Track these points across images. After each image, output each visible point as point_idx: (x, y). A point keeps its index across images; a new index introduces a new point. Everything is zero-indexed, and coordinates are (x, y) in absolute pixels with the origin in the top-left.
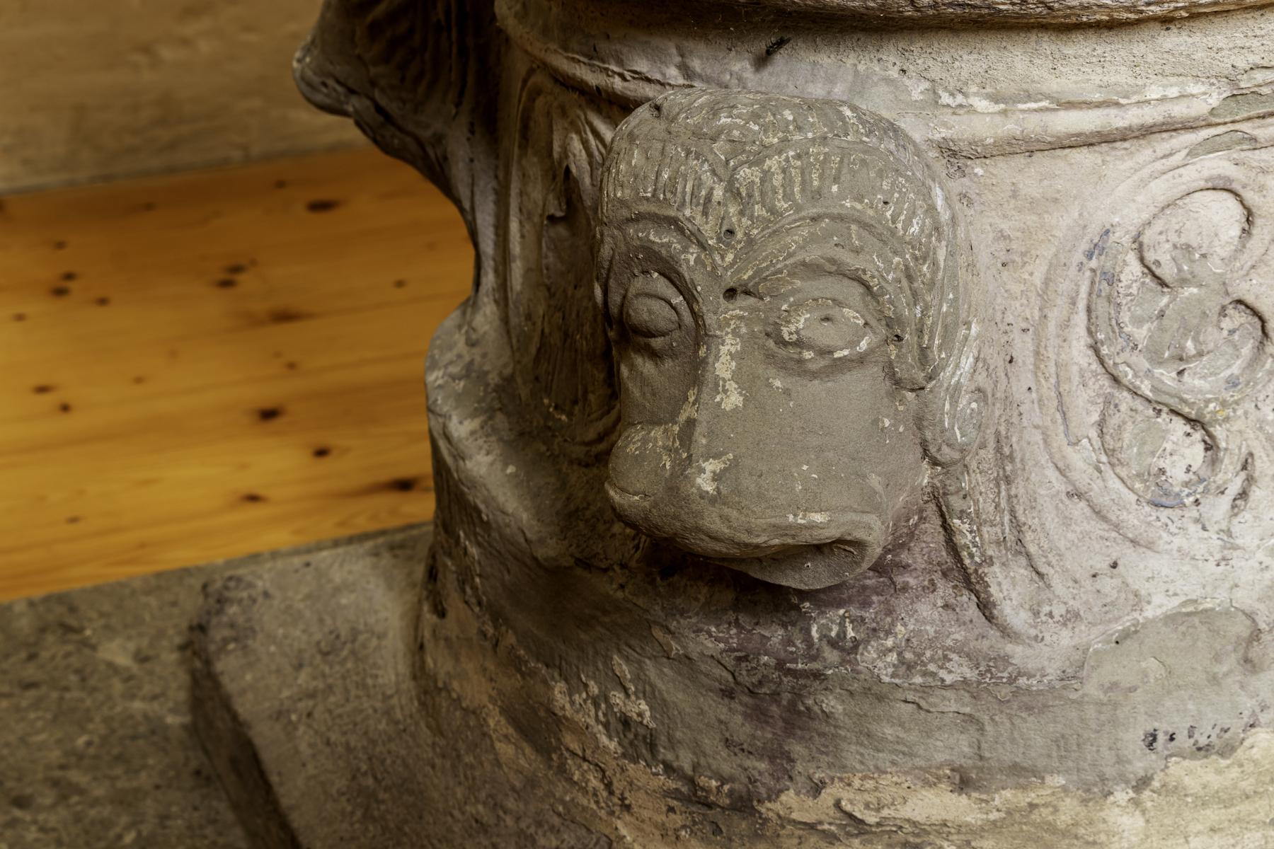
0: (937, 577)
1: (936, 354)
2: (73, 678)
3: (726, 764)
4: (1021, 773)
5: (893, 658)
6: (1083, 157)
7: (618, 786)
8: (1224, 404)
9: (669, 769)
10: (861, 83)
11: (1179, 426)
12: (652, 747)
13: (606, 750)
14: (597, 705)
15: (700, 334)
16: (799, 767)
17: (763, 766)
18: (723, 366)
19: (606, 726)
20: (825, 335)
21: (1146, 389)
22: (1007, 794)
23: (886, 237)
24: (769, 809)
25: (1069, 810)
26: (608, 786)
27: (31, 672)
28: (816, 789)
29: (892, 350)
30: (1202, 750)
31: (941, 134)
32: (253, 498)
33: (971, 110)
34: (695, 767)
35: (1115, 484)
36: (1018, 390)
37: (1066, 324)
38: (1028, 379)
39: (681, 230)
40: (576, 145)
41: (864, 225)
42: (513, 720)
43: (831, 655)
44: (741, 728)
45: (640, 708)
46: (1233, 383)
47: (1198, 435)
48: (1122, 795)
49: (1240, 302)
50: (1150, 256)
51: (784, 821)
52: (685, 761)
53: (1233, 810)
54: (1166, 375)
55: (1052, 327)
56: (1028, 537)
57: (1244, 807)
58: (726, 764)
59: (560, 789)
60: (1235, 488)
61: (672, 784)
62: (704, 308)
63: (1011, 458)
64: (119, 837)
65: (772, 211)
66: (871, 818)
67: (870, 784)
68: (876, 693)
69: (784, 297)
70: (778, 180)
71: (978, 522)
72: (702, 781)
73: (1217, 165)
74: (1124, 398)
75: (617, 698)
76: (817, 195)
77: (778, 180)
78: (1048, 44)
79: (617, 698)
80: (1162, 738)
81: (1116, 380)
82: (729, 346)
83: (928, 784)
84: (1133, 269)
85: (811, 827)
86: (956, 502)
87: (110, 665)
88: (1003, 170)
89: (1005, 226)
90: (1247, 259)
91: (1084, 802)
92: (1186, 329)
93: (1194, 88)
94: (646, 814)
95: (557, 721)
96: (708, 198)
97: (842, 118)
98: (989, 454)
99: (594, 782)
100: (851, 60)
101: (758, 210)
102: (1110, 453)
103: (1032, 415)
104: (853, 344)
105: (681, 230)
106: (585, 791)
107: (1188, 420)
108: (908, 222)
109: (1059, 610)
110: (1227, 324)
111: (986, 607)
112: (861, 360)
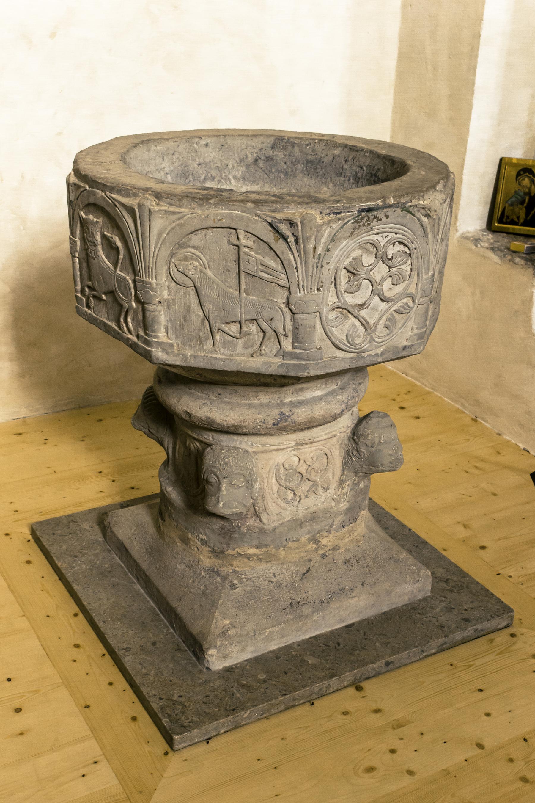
0: (253, 516)
1: (254, 484)
2: (78, 532)
3: (219, 545)
4: (267, 546)
6: (274, 453)
7: (200, 550)
8: (296, 487)
9: (209, 547)
10: (241, 443)
11: (289, 491)
12: (206, 543)
13: (198, 544)
14: (197, 537)
15: (220, 483)
16: (231, 546)
17: (225, 546)
18: (223, 488)
19: (198, 540)
20: (238, 483)
21: (284, 486)
22: (264, 549)
23: (247, 469)
24: (226, 553)
25: (273, 551)
26: (199, 550)
27: (69, 531)
28: (234, 549)
29: (247, 484)
30: (294, 541)
31: (253, 450)
32: (101, 492)
33: (258, 446)
34: (214, 546)
35: (280, 500)
36: (265, 487)
37: (272, 477)
38: (266, 485)
39: (217, 468)
40: (192, 445)
41: (243, 467)
42: (181, 540)
43: (237, 528)
44: (222, 540)
45: (205, 537)
47: (292, 492)
48: (282, 548)
49: (298, 472)
50: (285, 466)
51: (229, 554)
52: (212, 545)
53: (352, 258)
54: (288, 484)
55: (270, 477)
56: (267, 509)
58: (219, 545)
59: (190, 550)
60: (298, 500)
61: (210, 549)
62: (220, 479)
63: (264, 497)
64: (96, 562)
65: (230, 466)
66: (243, 554)
67: (242, 548)
68: (244, 534)
69: (232, 478)
70: (231, 461)
71: (259, 507)
72: (215, 549)
73: (295, 452)
74: (281, 488)
75: (201, 536)
76: (237, 463)
77: (231, 461)
78: (269, 437)
79: (201, 536)
80: (288, 540)
82: (224, 485)
83: (251, 548)
84: (282, 468)
85: (233, 555)
86: (256, 505)
87: (85, 529)
88: (263, 455)
91: (276, 550)
92: (290, 477)
93: (291, 442)
94: (205, 554)
95: (189, 539)
96: (221, 464)
97: (240, 451)
98: (261, 497)
99: (196, 549)
100: (239, 438)
101: (228, 466)
102: (279, 495)
103: (267, 491)
104: (242, 484)
105: (217, 468)
106: (194, 551)
107: (291, 490)
108: (250, 466)
109: (272, 520)
110: (296, 475)
111: (261, 520)
112: (243, 486)
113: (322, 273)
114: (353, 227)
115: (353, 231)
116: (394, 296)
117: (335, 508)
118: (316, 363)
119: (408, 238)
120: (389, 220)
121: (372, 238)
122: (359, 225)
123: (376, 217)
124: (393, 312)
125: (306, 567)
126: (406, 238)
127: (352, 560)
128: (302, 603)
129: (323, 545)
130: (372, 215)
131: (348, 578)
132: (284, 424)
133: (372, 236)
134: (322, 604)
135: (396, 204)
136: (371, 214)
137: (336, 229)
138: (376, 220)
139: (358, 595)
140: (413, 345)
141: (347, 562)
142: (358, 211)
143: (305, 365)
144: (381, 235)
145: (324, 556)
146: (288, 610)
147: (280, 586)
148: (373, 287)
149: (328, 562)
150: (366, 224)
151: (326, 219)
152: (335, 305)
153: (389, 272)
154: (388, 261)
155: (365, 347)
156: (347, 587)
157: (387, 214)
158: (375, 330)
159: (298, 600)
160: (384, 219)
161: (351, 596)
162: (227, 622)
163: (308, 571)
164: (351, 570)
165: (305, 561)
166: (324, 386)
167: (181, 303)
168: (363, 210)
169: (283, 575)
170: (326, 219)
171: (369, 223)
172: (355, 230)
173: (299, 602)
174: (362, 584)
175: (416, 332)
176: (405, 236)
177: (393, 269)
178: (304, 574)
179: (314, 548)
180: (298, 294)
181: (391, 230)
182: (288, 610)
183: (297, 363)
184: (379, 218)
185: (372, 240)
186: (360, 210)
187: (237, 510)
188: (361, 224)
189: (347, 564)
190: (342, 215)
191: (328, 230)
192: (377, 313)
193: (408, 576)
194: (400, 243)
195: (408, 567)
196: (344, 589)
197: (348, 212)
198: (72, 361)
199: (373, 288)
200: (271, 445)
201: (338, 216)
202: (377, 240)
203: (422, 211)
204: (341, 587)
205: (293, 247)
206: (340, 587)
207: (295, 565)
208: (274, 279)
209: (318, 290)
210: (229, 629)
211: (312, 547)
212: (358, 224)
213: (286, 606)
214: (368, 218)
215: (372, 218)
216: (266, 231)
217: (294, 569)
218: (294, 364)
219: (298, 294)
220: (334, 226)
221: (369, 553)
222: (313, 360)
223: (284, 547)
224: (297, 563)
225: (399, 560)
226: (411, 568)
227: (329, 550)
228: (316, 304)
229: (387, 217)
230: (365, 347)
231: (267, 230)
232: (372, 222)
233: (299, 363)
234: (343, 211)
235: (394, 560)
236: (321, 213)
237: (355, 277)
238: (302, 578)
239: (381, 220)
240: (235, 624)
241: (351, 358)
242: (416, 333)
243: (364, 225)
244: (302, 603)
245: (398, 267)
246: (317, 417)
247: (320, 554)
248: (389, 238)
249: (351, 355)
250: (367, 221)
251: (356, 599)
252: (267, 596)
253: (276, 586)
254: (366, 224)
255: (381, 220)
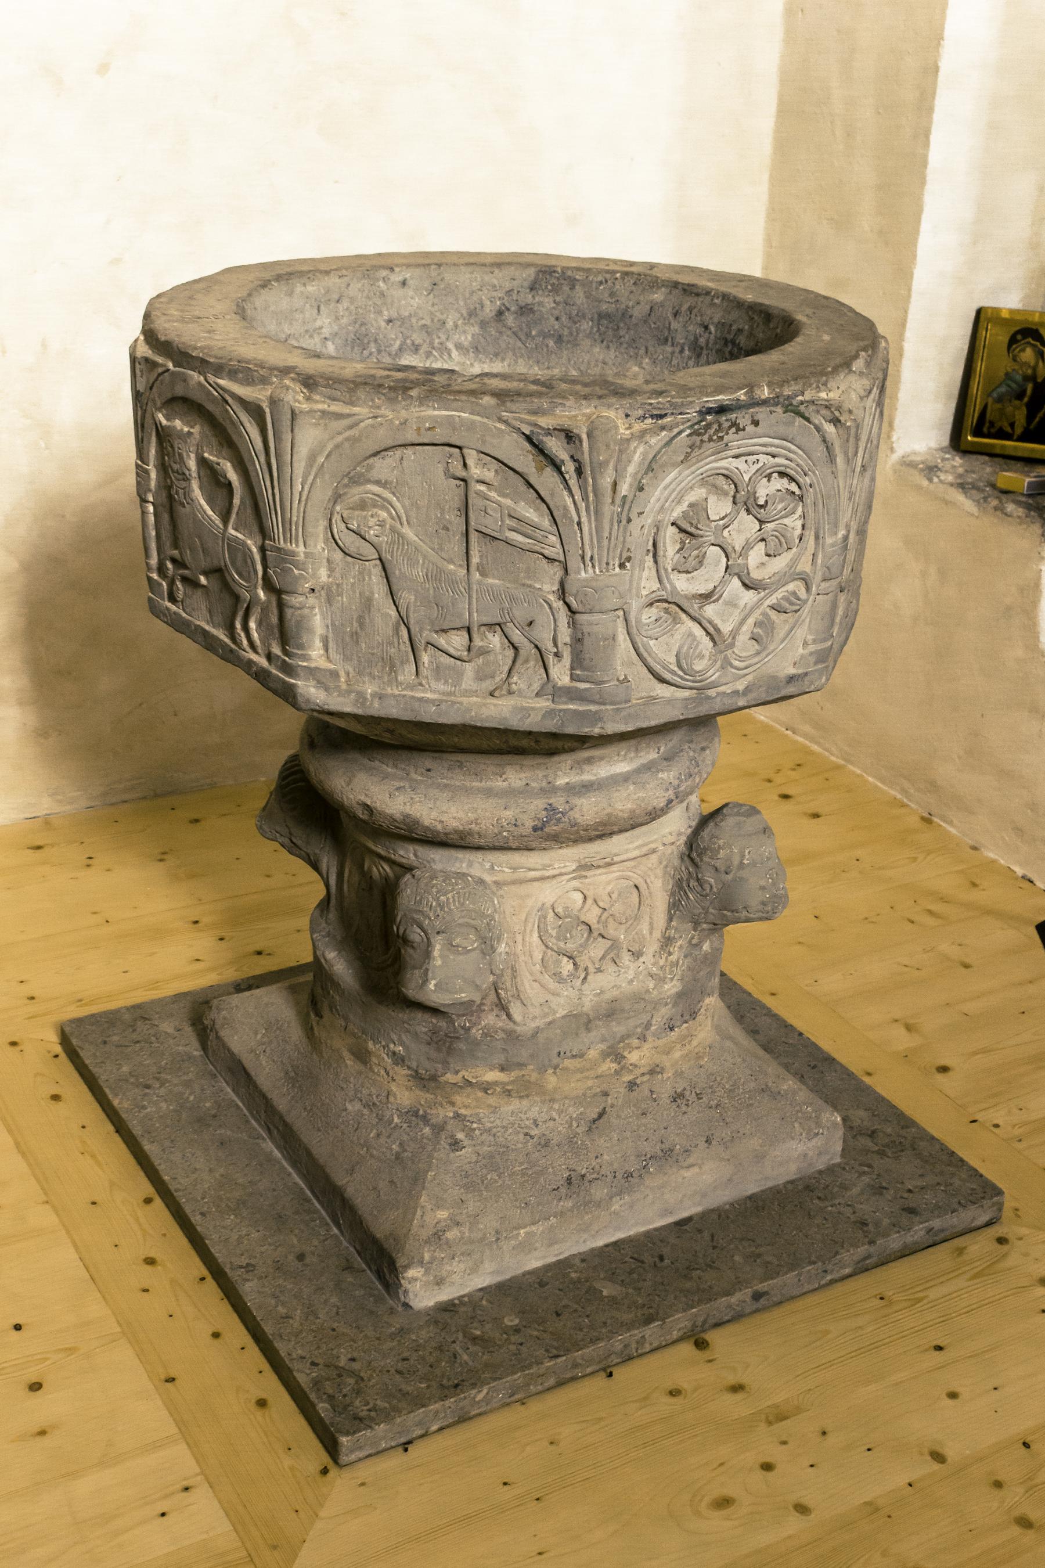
0: (494, 1007)
2: (153, 1039)
3: (427, 1064)
4: (521, 1065)
5: (481, 1032)
6: (535, 884)
7: (391, 1074)
8: (579, 952)
9: (409, 1068)
10: (470, 864)
11: (565, 959)
12: (403, 1061)
13: (387, 1062)
14: (384, 1049)
15: (429, 944)
16: (452, 1065)
17: (440, 1066)
18: (436, 953)
19: (387, 1055)
20: (465, 943)
21: (555, 948)
22: (516, 1072)
23: (483, 915)
24: (442, 1079)
25: (534, 1076)
26: (388, 1074)
27: (134, 1036)
28: (457, 1072)
30: (574, 1057)
31: (495, 878)
32: (198, 960)
33: (503, 872)
34: (417, 1067)
35: (547, 977)
36: (518, 951)
37: (532, 931)
38: (520, 947)
39: (423, 914)
40: (375, 869)
41: (476, 912)
42: (353, 1054)
43: (462, 1032)
44: (433, 1054)
45: (400, 1049)
46: (581, 946)
47: (571, 961)
48: (550, 1071)
49: (583, 922)
50: (556, 911)
51: (447, 1082)
52: (414, 1065)
53: (687, 503)
54: (562, 944)
55: (528, 931)
56: (521, 994)
57: (587, 1074)
58: (427, 1064)
59: (370, 1075)
60: (582, 976)
61: (409, 1072)
62: (431, 936)
64: (188, 1098)
65: (450, 909)
67: (473, 1070)
68: (477, 1044)
70: (451, 900)
71: (506, 990)
72: (420, 1071)
74: (549, 952)
75: (392, 1046)
77: (451, 900)
78: (526, 853)
79: (392, 1046)
80: (562, 1054)
81: (547, 947)
82: (438, 947)
83: (491, 1070)
84: (551, 914)
85: (455, 1084)
86: (500, 985)
88: (513, 888)
89: (513, 904)
90: (585, 910)
91: (539, 1073)
92: (567, 931)
93: (568, 864)
94: (400, 1082)
95: (368, 1053)
96: (431, 906)
97: (468, 880)
98: (509, 971)
99: (382, 1072)
100: (467, 856)
101: (446, 909)
102: (545, 967)
103: (522, 958)
105: (423, 914)
106: (379, 1075)
107: (568, 957)
108: (488, 910)
109: (531, 1016)
111: (509, 1016)
112: (474, 949)
113: (628, 534)
114: (690, 443)
115: (689, 450)
116: (770, 578)
117: (655, 992)
118: (618, 709)
119: (797, 465)
120: (759, 430)
121: (727, 465)
122: (701, 440)
123: (734, 424)
124: (768, 610)
125: (598, 1107)
126: (793, 465)
127: (687, 1093)
128: (589, 1177)
129: (631, 1065)
130: (727, 420)
131: (681, 1128)
132: (555, 828)
133: (726, 460)
134: (630, 1179)
135: (773, 398)
136: (724, 418)
137: (657, 448)
138: (733, 430)
139: (700, 1162)
140: (806, 674)
141: (677, 1097)
142: (700, 412)
143: (596, 712)
144: (744, 458)
145: (632, 1085)
146: (563, 1190)
147: (546, 1145)
148: (728, 560)
149: (640, 1098)
150: (715, 437)
151: (638, 427)
152: (654, 595)
153: (760, 530)
154: (759, 510)
155: (713, 678)
156: (678, 1147)
157: (756, 418)
158: (732, 645)
159: (583, 1172)
160: (750, 429)
161: (686, 1164)
162: (442, 1214)
163: (601, 1115)
164: (685, 1113)
165: (595, 1095)
166: (632, 754)
167: (354, 592)
168: (709, 411)
169: (552, 1122)
170: (638, 427)
171: (720, 435)
172: (693, 450)
173: (583, 1176)
174: (707, 1141)
175: (812, 648)
176: (791, 461)
177: (768, 525)
178: (594, 1121)
179: (613, 1070)
180: (583, 574)
181: (764, 449)
182: (563, 1190)
183: (581, 708)
184: (741, 426)
185: (727, 469)
186: (704, 409)
187: (463, 995)
188: (706, 438)
189: (679, 1101)
190: (669, 419)
191: (641, 449)
192: (737, 612)
193: (796, 1125)
194: (782, 474)
195: (798, 1108)
196: (672, 1151)
197: (681, 414)
198: (140, 705)
199: (729, 563)
200: (530, 870)
201: (660, 422)
202: (737, 468)
203: (824, 412)
204: (666, 1146)
205: (573, 482)
206: (663, 1146)
207: (575, 1104)
208: (535, 545)
209: (622, 566)
210: (448, 1228)
211: (609, 1069)
212: (700, 438)
213: (559, 1184)
214: (720, 426)
215: (726, 425)
216: (519, 452)
217: (574, 1112)
218: (575, 711)
219: (583, 574)
220: (653, 441)
221: (721, 1080)
222: (612, 704)
223: (556, 1067)
224: (580, 1100)
225: (779, 1093)
226: (804, 1110)
227: (643, 1074)
228: (617, 593)
229: (756, 423)
230: (713, 678)
231: (522, 449)
232: (727, 434)
233: (585, 708)
234: (670, 412)
235: (769, 1093)
236: (627, 416)
237: (694, 541)
238: (590, 1129)
239: (744, 429)
240: (459, 1218)
241: (686, 699)
242: (813, 650)
243: (710, 440)
244: (589, 1177)
245: (777, 522)
246: (620, 814)
247: (624, 1082)
248: (761, 464)
249: (687, 693)
250: (717, 431)
251: (696, 1169)
252: (521, 1164)
253: (539, 1144)
254: (715, 437)
255: (744, 429)
